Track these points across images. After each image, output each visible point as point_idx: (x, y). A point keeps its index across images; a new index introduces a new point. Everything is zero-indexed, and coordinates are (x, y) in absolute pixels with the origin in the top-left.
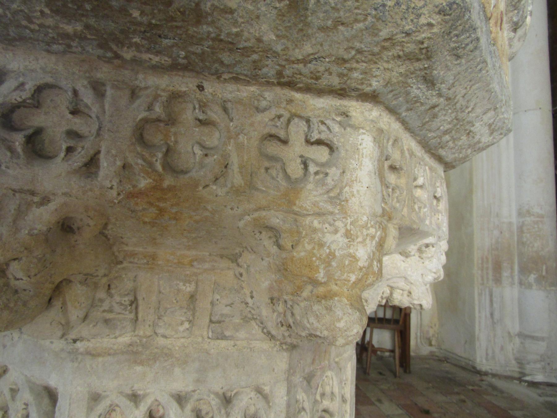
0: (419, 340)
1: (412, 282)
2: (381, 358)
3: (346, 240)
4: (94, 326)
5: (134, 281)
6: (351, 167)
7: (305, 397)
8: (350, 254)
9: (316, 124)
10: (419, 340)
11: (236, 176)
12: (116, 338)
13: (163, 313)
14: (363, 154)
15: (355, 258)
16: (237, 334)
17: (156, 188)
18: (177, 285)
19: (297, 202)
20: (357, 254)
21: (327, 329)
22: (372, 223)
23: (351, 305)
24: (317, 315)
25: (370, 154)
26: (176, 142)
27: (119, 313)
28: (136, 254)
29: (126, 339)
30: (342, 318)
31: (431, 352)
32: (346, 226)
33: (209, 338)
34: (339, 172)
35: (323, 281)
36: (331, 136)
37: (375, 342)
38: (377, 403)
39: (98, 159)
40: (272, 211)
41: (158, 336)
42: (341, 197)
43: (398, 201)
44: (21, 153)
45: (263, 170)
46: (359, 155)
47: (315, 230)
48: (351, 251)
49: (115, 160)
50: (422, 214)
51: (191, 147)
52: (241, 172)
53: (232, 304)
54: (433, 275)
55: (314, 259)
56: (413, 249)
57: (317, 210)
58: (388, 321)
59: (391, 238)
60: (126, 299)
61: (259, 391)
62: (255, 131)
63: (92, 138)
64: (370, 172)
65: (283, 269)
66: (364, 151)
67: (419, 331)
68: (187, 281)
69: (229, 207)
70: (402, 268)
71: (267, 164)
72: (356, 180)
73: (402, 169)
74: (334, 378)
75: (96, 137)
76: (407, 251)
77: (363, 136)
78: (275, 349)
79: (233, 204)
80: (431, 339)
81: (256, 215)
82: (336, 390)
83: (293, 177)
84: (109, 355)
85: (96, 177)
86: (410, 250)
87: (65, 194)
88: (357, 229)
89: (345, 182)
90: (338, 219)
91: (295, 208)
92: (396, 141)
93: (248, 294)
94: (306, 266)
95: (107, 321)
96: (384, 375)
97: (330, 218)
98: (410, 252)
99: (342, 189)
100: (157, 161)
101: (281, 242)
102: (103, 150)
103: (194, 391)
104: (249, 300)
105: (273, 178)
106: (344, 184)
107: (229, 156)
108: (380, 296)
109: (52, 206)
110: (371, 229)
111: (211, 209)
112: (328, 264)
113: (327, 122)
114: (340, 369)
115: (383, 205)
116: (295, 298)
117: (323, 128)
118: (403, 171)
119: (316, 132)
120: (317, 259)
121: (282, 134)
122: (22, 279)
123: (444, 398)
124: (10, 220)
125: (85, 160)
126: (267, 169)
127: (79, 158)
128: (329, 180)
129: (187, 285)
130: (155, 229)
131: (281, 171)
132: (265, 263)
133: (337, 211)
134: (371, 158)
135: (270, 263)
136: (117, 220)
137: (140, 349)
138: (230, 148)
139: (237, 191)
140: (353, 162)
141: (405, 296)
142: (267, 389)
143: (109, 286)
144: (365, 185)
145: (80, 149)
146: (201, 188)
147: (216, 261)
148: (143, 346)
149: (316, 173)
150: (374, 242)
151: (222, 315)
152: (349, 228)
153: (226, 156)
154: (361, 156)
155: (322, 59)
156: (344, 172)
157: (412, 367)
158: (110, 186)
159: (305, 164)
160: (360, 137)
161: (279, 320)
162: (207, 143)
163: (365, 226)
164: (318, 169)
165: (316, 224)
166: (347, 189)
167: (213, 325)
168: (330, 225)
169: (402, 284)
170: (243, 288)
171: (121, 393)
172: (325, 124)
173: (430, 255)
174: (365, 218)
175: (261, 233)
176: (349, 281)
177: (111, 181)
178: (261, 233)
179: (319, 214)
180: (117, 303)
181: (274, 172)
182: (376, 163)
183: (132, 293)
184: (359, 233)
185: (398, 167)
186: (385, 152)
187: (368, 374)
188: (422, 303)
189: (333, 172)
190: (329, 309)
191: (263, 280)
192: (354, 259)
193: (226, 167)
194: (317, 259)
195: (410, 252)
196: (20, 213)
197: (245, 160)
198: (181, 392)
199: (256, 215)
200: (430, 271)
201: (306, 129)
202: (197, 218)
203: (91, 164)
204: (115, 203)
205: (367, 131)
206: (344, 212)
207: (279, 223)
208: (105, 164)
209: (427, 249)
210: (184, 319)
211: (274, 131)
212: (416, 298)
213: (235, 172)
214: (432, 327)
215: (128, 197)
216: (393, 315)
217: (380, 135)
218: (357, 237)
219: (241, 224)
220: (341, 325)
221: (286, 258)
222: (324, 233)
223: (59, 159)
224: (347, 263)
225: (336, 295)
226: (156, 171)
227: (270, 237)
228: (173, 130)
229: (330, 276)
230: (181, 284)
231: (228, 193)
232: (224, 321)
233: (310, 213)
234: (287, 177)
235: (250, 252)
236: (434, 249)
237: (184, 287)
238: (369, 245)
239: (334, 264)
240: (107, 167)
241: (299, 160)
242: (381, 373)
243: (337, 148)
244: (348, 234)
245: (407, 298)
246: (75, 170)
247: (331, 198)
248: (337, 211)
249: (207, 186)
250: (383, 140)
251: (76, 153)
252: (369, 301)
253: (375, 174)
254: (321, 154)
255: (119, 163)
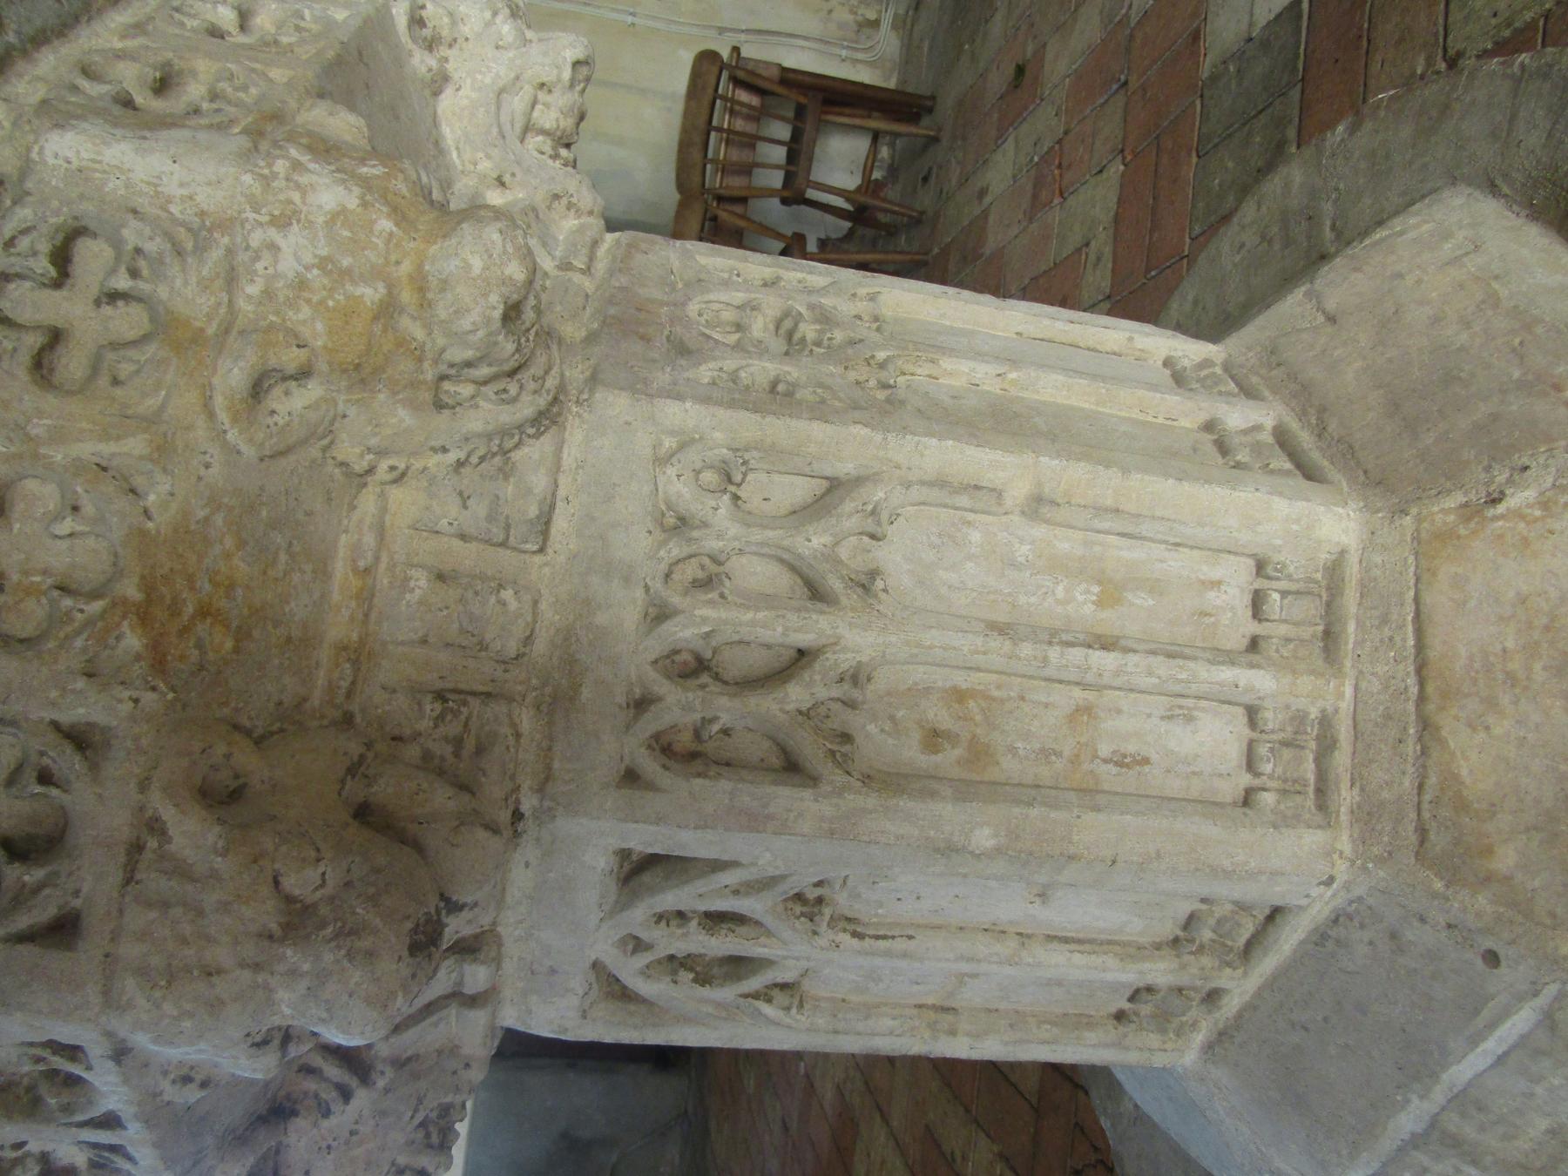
0: (860, 56)
1: (512, 75)
2: (893, 171)
3: (295, 227)
4: (484, 774)
5: (394, 691)
6: (122, 192)
7: (711, 365)
8: (326, 222)
9: (13, 259)
10: (860, 56)
11: (125, 449)
12: (518, 735)
13: (475, 640)
14: (93, 161)
15: (338, 213)
16: (536, 491)
17: (143, 616)
18: (408, 605)
19: (198, 324)
20: (328, 208)
21: (485, 295)
22: (262, 164)
23: (444, 237)
24: (456, 312)
25: (94, 144)
26: (45, 572)
27: (466, 725)
28: (330, 682)
29: (524, 716)
30: (464, 260)
31: (894, 27)
32: (261, 224)
33: (541, 550)
34: (134, 222)
35: (382, 289)
36: (44, 229)
37: (851, 182)
38: (987, 200)
39: (72, 726)
40: (216, 381)
41: (524, 654)
42: (195, 226)
43: (245, 88)
44: (48, 869)
45: (118, 392)
46: (96, 170)
47: (268, 294)
48: (321, 219)
49: (73, 691)
50: (315, 27)
51: (59, 542)
52: (118, 438)
53: (461, 494)
54: (499, 19)
55: (331, 303)
56: (422, 61)
57: (219, 283)
58: (796, 136)
59: (331, 120)
60: (428, 708)
61: (661, 461)
62: (21, 400)
63: (21, 735)
64: (137, 150)
65: (362, 374)
66: (85, 155)
67: (837, 51)
68: (404, 584)
69: (202, 472)
70: (474, 95)
71: (103, 381)
72: (156, 186)
73: (168, 64)
74: (711, 297)
75: (18, 728)
76: (429, 76)
77: (48, 153)
78: (586, 415)
79: (195, 462)
80: (860, 18)
81: (223, 417)
82: (739, 297)
83: (146, 326)
84: (550, 749)
85: (110, 729)
86: (424, 69)
87: (144, 786)
88: (271, 198)
89: (159, 212)
90: (245, 239)
91: (211, 331)
92: (86, 72)
93: (439, 457)
94: (347, 323)
95: (480, 751)
96: (930, 169)
97: (243, 257)
98: (430, 70)
99: (175, 221)
100: (82, 611)
101: (291, 368)
102: (48, 715)
103: (647, 588)
104: (452, 457)
105: (138, 372)
106: (163, 215)
107: (79, 459)
108: (550, 162)
109: (168, 814)
110: (275, 169)
111: (207, 511)
112: (346, 274)
113: (8, 235)
114: (699, 283)
115: (237, 130)
116: (429, 355)
117: (24, 243)
118: (176, 61)
119: (31, 263)
120: (331, 297)
121: (34, 341)
122: (324, 874)
123: (999, 17)
124: (189, 887)
125: (69, 749)
126: (116, 382)
127: (67, 761)
128: (151, 247)
129: (412, 584)
130: (256, 633)
131: (122, 352)
132: (352, 412)
133: (226, 240)
134: (104, 143)
135: (348, 401)
136: (226, 704)
137: (548, 690)
138: (59, 457)
139: (163, 452)
140: (111, 185)
141: (549, 98)
142: (669, 443)
143: (393, 739)
144: (168, 166)
145: (46, 761)
146: (150, 525)
147: (361, 521)
148: (544, 685)
149: (134, 273)
150: (312, 166)
151: (490, 518)
152: (267, 218)
153: (78, 467)
154: (97, 166)
155: (436, 195)
156: (135, 212)
157: (924, 90)
158: (131, 704)
159: (114, 297)
160: (51, 161)
161: (494, 397)
162: (51, 507)
163: (266, 181)
164: (123, 269)
165: (253, 290)
166: (175, 209)
167: (511, 538)
168: (257, 258)
169: (517, 103)
170: (425, 468)
171: (628, 727)
172: (13, 238)
173: (446, 20)
174: (247, 179)
175: (273, 412)
176: (391, 234)
177: (120, 701)
178: (273, 412)
179: (231, 279)
180: (436, 726)
181: (125, 369)
182: (119, 132)
183: (418, 696)
184: (282, 197)
185: (158, 75)
186: (100, 104)
187: (922, 213)
188: (570, 61)
189: (132, 234)
190: (445, 285)
191: (394, 421)
192: (339, 215)
193: (105, 469)
194: (331, 297)
195: (430, 70)
196: (182, 871)
197: (90, 426)
198: (646, 614)
199: (223, 417)
200: (488, 24)
201: (28, 284)
202: (229, 542)
203: (80, 739)
204: (175, 699)
205: (36, 142)
206: (226, 224)
207: (241, 369)
208: (81, 711)
209: (430, 25)
210: (493, 600)
211: (25, 358)
212: (555, 72)
213: (117, 450)
214: (830, 12)
215: (163, 672)
216: (783, 119)
217: (56, 112)
218: (290, 202)
219: (249, 452)
220: (477, 264)
221: (330, 364)
222: (276, 276)
223: (66, 799)
224: (346, 233)
225: (420, 266)
226: (105, 611)
227: (287, 393)
228: (15, 577)
229: (376, 274)
230: (408, 596)
231: (165, 470)
232: (507, 517)
233: (226, 300)
234: (145, 339)
235: (332, 442)
236: (429, 6)
237: (418, 591)
238: (314, 178)
239: (346, 262)
240: (86, 708)
241: (107, 310)
242: (925, 179)
243: (76, 218)
244: (282, 222)
245: (557, 93)
246: (90, 769)
247: (196, 248)
248: (226, 240)
249: (146, 512)
250: (68, 103)
251: (55, 768)
252: (558, 189)
253: (145, 138)
254: (92, 257)
255: (81, 684)
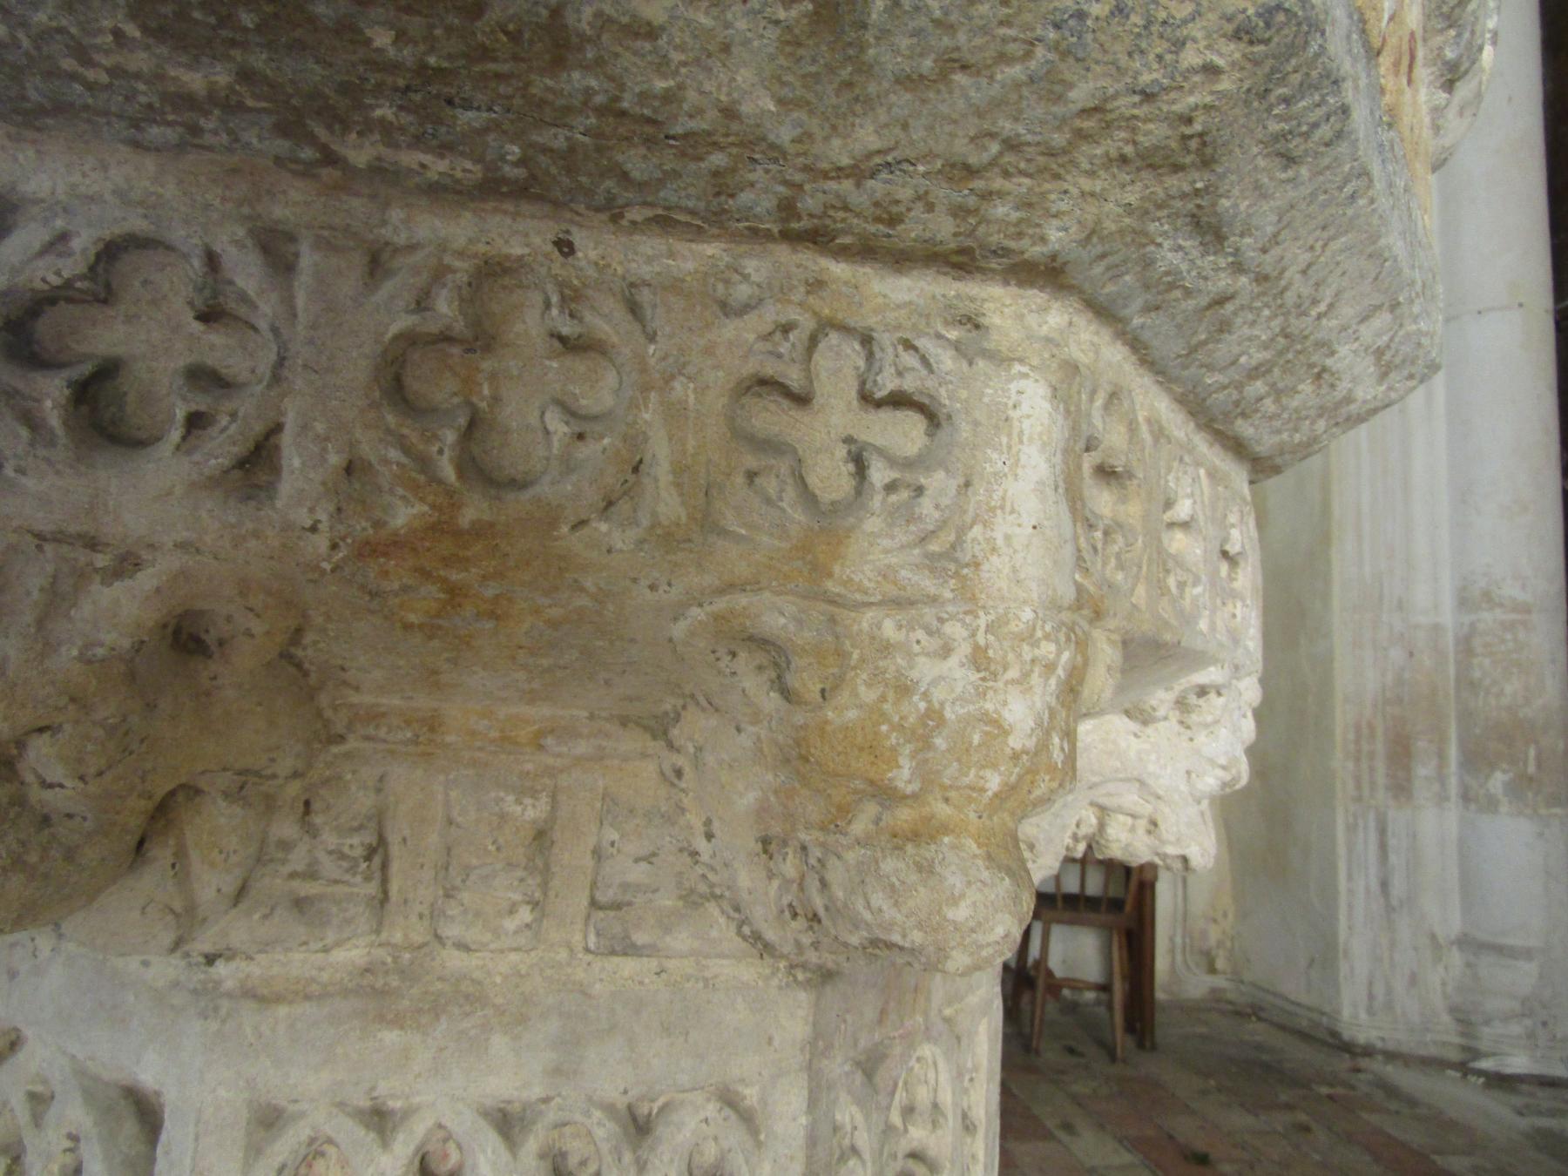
0: (1179, 958)
1: (1161, 793)
2: (1073, 1008)
3: (974, 676)
4: (265, 917)
5: (379, 791)
6: (989, 469)
7: (859, 1118)
8: (986, 714)
9: (890, 350)
10: (1179, 958)
11: (664, 494)
12: (326, 950)
13: (458, 882)
14: (1021, 433)
15: (1000, 727)
16: (668, 939)
17: (440, 528)
18: (498, 800)
19: (837, 569)
20: (1006, 714)
21: (920, 926)
22: (1048, 628)
23: (989, 857)
24: (892, 886)
25: (1040, 434)
26: (496, 399)
27: (336, 882)
28: (384, 715)
29: (355, 952)
30: (963, 896)
31: (1214, 991)
32: (973, 635)
33: (587, 950)
34: (953, 484)
35: (909, 789)
36: (931, 383)
37: (1055, 964)
38: (1061, 1135)
39: (277, 448)
40: (767, 594)
41: (444, 945)
42: (959, 554)
43: (1121, 566)
44: (60, 431)
45: (740, 479)
46: (1009, 435)
47: (886, 648)
48: (989, 706)
49: (324, 449)
50: (1187, 603)
51: (537, 413)
52: (678, 485)
53: (654, 855)
54: (1220, 773)
55: (884, 728)
56: (1162, 701)
57: (892, 591)
58: (1092, 903)
59: (1102, 670)
60: (356, 840)
61: (729, 1099)
62: (716, 367)
63: (259, 388)
64: (1041, 483)
65: (796, 757)
66: (1026, 424)
67: (1179, 931)
68: (526, 791)
69: (644, 583)
70: (1132, 754)
71: (751, 461)
72: (1002, 508)
73: (1131, 476)
74: (941, 1065)
75: (269, 387)
76: (1147, 707)
77: (1023, 384)
78: (775, 982)
79: (656, 574)
80: (1214, 953)
81: (721, 604)
82: (946, 1098)
83: (826, 497)
84: (307, 998)
85: (271, 498)
86: (1154, 702)
87: (182, 546)
88: (1006, 644)
89: (971, 513)
90: (952, 617)
91: (831, 586)
92: (1114, 396)
93: (699, 827)
94: (861, 749)
95: (300, 904)
96: (1081, 1055)
97: (929, 613)
98: (1154, 709)
99: (962, 531)
100: (441, 452)
101: (792, 680)
102: (291, 422)
103: (546, 1100)
104: (701, 844)
105: (768, 501)
106: (968, 518)
107: (646, 440)
108: (1069, 833)
109: (146, 580)
110: (1043, 643)
111: (593, 589)
112: (924, 742)
113: (920, 343)
114: (957, 1039)
115: (1077, 577)
116: (831, 839)
117: (909, 359)
118: (1135, 482)
119: (889, 371)
120: (893, 728)
121: (794, 377)
122: (61, 786)
123: (1250, 1120)
124: (29, 618)
125: (238, 450)
126: (751, 476)
127: (223, 445)
128: (926, 506)
129: (528, 801)
130: (435, 643)
131: (790, 481)
132: (745, 740)
133: (948, 595)
134: (1044, 445)
135: (759, 739)
136: (328, 618)
137: (394, 981)
138: (647, 416)
139: (667, 539)
140: (995, 456)
141: (1141, 831)
142: (751, 1095)
143: (307, 804)
144: (1028, 521)
145: (224, 420)
146: (565, 529)
147: (607, 736)
148: (402, 972)
149: (891, 487)
150: (1053, 681)
151: (625, 886)
152: (982, 642)
153: (635, 440)
154: (1015, 438)
155: (905, 166)
156: (967, 484)
157: (1159, 1034)
158: (308, 523)
159: (859, 463)
160: (1013, 387)
161: (785, 902)
162: (583, 402)
163: (1028, 636)
164: (895, 475)
165: (889, 629)
166: (977, 531)
167: (601, 914)
168: (930, 633)
169: (1130, 798)
170: (683, 810)
171: (341, 1105)
172: (916, 349)
173: (1209, 719)
174: (1027, 614)
175: (734, 655)
176: (983, 790)
177: (312, 510)
178: (734, 655)
179: (898, 603)
180: (330, 853)
181: (770, 485)
182: (1058, 458)
183: (373, 825)
184: (1011, 657)
185: (1119, 469)
186: (1084, 427)
187: (1037, 1052)
188: (1187, 852)
189: (938, 483)
190: (926, 869)
191: (740, 787)
192: (997, 727)
193: (636, 470)
194: (893, 728)
195: (1154, 709)
196: (57, 600)
197: (691, 450)
198: (509, 1102)
199: (721, 604)
200: (1211, 761)
201: (862, 363)
202: (555, 612)
203: (257, 462)
204: (323, 572)
205: (1033, 368)
206: (969, 597)
207: (785, 627)
208: (297, 462)
209: (1201, 702)
210: (517, 897)
211: (770, 369)
212: (1172, 839)
213: (662, 484)
214: (1215, 921)
215: (360, 555)
216: (1106, 886)
217: (1069, 380)
218: (1005, 668)
219: (679, 630)
220: (960, 913)
221: (804, 727)
222: (911, 656)
223: (166, 448)
224: (976, 739)
225: (945, 829)
226: (440, 482)
227: (760, 668)
228: (486, 365)
229: (928, 778)
230: (511, 798)
231: (641, 542)
232: (630, 904)
233: (872, 599)
234: (808, 497)
235: (703, 710)
236: (1222, 700)
237: (519, 809)
238: (1038, 690)
239: (940, 742)
240: (301, 470)
241: (841, 451)
242: (1071, 1051)
243: (949, 417)
244: (979, 659)
245: (1146, 839)
246: (210, 478)
247: (931, 556)
248: (948, 595)
249: (582, 523)
250: (1079, 393)
251: (213, 431)
252: (1040, 847)
253: (1056, 489)
254: (902, 434)
255: (335, 459)
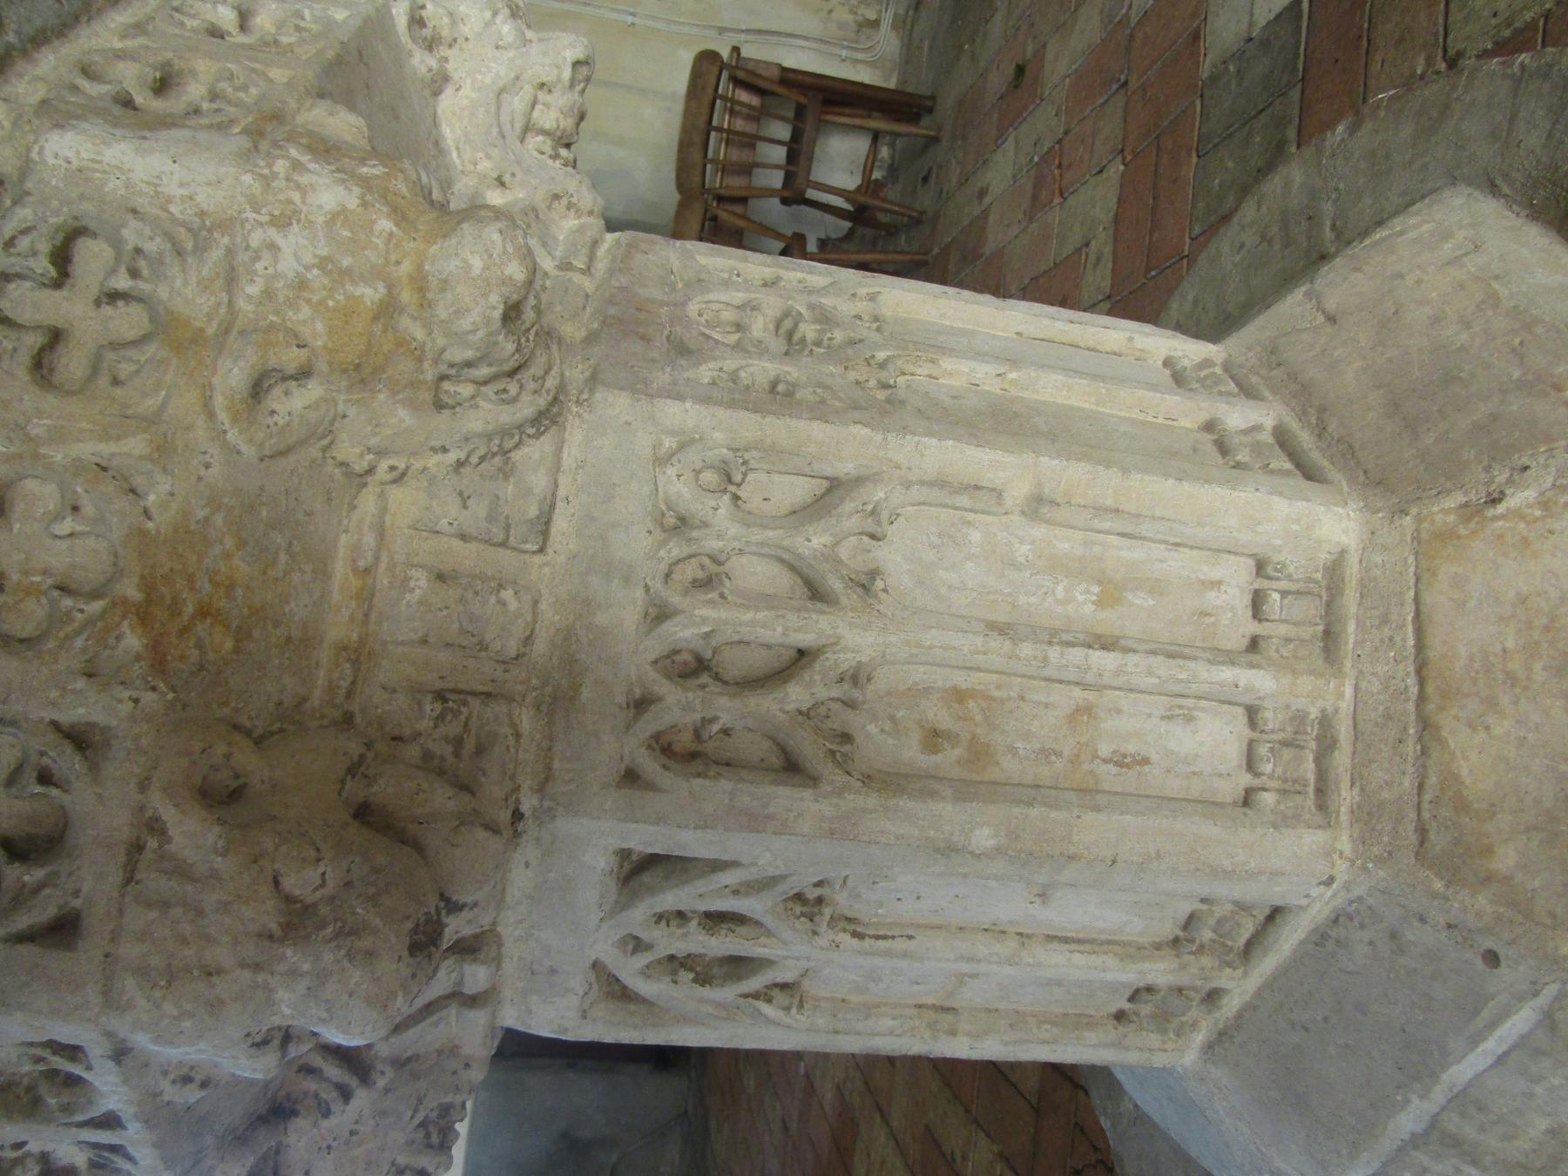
0: (860, 56)
1: (512, 75)
2: (893, 171)
3: (295, 227)
4: (484, 774)
5: (394, 691)
6: (122, 192)
7: (711, 365)
8: (326, 222)
9: (13, 259)
10: (860, 56)
11: (125, 449)
12: (518, 735)
13: (475, 640)
14: (93, 161)
15: (338, 213)
16: (536, 491)
17: (143, 616)
18: (408, 605)
19: (198, 324)
20: (328, 208)
21: (485, 295)
22: (262, 164)
23: (444, 237)
24: (456, 312)
25: (94, 144)
26: (45, 572)
27: (466, 725)
28: (330, 682)
29: (524, 716)
30: (464, 260)
31: (894, 27)
32: (261, 224)
33: (541, 550)
34: (134, 222)
35: (382, 289)
36: (44, 229)
37: (851, 182)
38: (987, 200)
39: (72, 726)
40: (216, 381)
41: (524, 654)
42: (195, 226)
43: (245, 88)
44: (48, 869)
45: (118, 392)
46: (96, 170)
47: (268, 294)
48: (321, 219)
49: (73, 691)
50: (315, 27)
51: (59, 542)
52: (118, 438)
53: (461, 494)
54: (499, 19)
55: (331, 303)
56: (422, 61)
57: (219, 283)
58: (796, 136)
59: (331, 120)
60: (428, 708)
61: (661, 461)
62: (21, 400)
63: (21, 735)
64: (137, 150)
65: (362, 374)
66: (85, 155)
67: (837, 51)
68: (404, 584)
69: (202, 472)
70: (474, 95)
71: (103, 381)
72: (156, 186)
73: (168, 64)
74: (711, 297)
75: (18, 728)
76: (429, 76)
77: (48, 153)
78: (586, 415)
79: (195, 462)
80: (860, 18)
81: (223, 417)
82: (739, 297)
83: (146, 326)
84: (550, 749)
85: (110, 729)
86: (424, 69)
87: (144, 786)
88: (271, 198)
89: (159, 212)
90: (245, 239)
91: (211, 331)
92: (86, 72)
93: (439, 457)
94: (347, 323)
95: (480, 751)
96: (930, 169)
97: (243, 257)
98: (430, 70)
99: (175, 221)
100: (82, 611)
101: (291, 368)
102: (48, 715)
103: (647, 588)
104: (452, 457)
105: (138, 372)
106: (163, 215)
107: (79, 459)
108: (550, 162)
109: (168, 814)
110: (275, 169)
111: (207, 511)
112: (346, 274)
113: (8, 235)
114: (699, 283)
115: (237, 130)
116: (429, 355)
117: (24, 243)
118: (176, 61)
119: (31, 263)
120: (331, 297)
121: (34, 341)
122: (324, 874)
123: (999, 17)
124: (189, 887)
125: (69, 749)
126: (116, 382)
127: (67, 761)
128: (151, 247)
129: (412, 584)
130: (256, 633)
131: (122, 352)
132: (352, 412)
133: (226, 240)
134: (104, 143)
135: (348, 401)
136: (226, 704)
137: (548, 690)
138: (59, 457)
139: (163, 452)
140: (111, 185)
141: (549, 98)
142: (669, 443)
143: (393, 739)
144: (168, 166)
145: (46, 761)
146: (150, 525)
147: (361, 521)
148: (544, 685)
149: (134, 273)
150: (312, 166)
151: (490, 518)
152: (267, 218)
153: (78, 467)
154: (97, 166)
155: (436, 195)
156: (135, 212)
157: (924, 90)
158: (131, 704)
159: (114, 297)
160: (51, 161)
161: (494, 397)
162: (51, 507)
163: (266, 181)
164: (123, 269)
165: (253, 290)
166: (175, 209)
167: (511, 538)
168: (257, 258)
169: (517, 103)
170: (425, 468)
171: (628, 727)
172: (13, 238)
173: (446, 20)
174: (247, 179)
175: (273, 412)
176: (391, 234)
177: (120, 701)
178: (273, 412)
179: (231, 279)
180: (436, 726)
181: (125, 369)
182: (119, 132)
183: (418, 696)
184: (282, 197)
185: (158, 75)
186: (100, 104)
187: (922, 213)
188: (570, 61)
189: (132, 234)
190: (445, 285)
191: (394, 421)
192: (339, 215)
193: (105, 469)
194: (331, 297)
195: (430, 70)
196: (182, 871)
197: (90, 426)
198: (646, 614)
199: (223, 417)
200: (488, 24)
201: (28, 284)
202: (229, 542)
203: (80, 739)
204: (175, 699)
205: (36, 142)
206: (226, 224)
207: (241, 369)
208: (81, 711)
209: (430, 25)
210: (493, 600)
211: (25, 358)
212: (555, 72)
213: (117, 450)
214: (830, 12)
215: (163, 672)
216: (783, 119)
217: (56, 112)
218: (290, 202)
219: (249, 452)
220: (477, 264)
221: (330, 364)
222: (276, 276)
223: (66, 799)
224: (346, 233)
225: (420, 266)
226: (105, 611)
227: (287, 393)
228: (15, 577)
229: (376, 274)
230: (408, 596)
231: (165, 470)
232: (507, 517)
233: (226, 300)
234: (145, 339)
235: (332, 442)
236: (429, 6)
237: (418, 591)
238: (314, 178)
239: (346, 262)
240: (86, 708)
241: (107, 310)
242: (925, 179)
243: (76, 218)
244: (282, 222)
245: (557, 93)
246: (90, 769)
247: (196, 248)
248: (226, 240)
249: (146, 512)
250: (68, 103)
251: (55, 768)
252: (558, 189)
253: (145, 138)
254: (92, 257)
255: (81, 684)
